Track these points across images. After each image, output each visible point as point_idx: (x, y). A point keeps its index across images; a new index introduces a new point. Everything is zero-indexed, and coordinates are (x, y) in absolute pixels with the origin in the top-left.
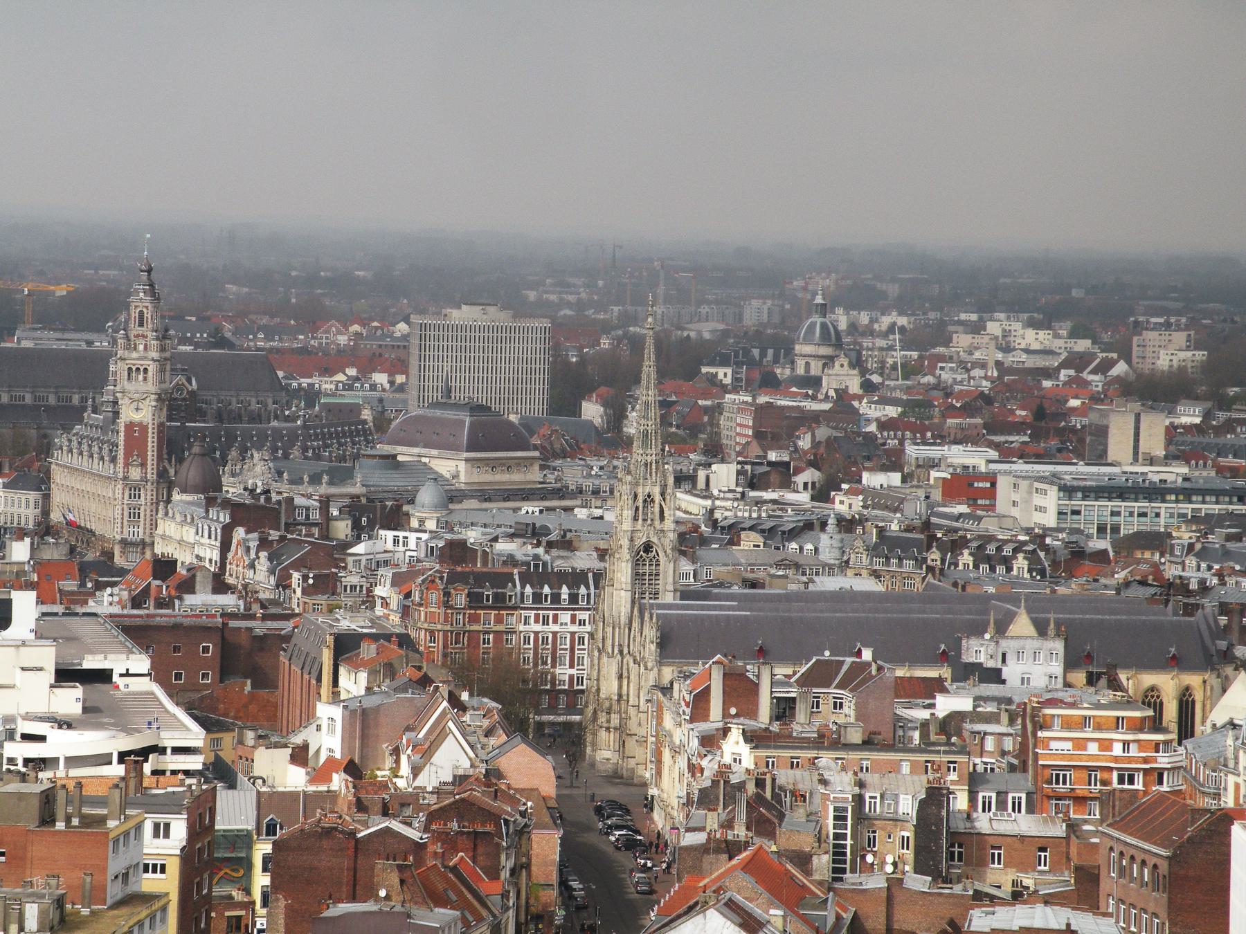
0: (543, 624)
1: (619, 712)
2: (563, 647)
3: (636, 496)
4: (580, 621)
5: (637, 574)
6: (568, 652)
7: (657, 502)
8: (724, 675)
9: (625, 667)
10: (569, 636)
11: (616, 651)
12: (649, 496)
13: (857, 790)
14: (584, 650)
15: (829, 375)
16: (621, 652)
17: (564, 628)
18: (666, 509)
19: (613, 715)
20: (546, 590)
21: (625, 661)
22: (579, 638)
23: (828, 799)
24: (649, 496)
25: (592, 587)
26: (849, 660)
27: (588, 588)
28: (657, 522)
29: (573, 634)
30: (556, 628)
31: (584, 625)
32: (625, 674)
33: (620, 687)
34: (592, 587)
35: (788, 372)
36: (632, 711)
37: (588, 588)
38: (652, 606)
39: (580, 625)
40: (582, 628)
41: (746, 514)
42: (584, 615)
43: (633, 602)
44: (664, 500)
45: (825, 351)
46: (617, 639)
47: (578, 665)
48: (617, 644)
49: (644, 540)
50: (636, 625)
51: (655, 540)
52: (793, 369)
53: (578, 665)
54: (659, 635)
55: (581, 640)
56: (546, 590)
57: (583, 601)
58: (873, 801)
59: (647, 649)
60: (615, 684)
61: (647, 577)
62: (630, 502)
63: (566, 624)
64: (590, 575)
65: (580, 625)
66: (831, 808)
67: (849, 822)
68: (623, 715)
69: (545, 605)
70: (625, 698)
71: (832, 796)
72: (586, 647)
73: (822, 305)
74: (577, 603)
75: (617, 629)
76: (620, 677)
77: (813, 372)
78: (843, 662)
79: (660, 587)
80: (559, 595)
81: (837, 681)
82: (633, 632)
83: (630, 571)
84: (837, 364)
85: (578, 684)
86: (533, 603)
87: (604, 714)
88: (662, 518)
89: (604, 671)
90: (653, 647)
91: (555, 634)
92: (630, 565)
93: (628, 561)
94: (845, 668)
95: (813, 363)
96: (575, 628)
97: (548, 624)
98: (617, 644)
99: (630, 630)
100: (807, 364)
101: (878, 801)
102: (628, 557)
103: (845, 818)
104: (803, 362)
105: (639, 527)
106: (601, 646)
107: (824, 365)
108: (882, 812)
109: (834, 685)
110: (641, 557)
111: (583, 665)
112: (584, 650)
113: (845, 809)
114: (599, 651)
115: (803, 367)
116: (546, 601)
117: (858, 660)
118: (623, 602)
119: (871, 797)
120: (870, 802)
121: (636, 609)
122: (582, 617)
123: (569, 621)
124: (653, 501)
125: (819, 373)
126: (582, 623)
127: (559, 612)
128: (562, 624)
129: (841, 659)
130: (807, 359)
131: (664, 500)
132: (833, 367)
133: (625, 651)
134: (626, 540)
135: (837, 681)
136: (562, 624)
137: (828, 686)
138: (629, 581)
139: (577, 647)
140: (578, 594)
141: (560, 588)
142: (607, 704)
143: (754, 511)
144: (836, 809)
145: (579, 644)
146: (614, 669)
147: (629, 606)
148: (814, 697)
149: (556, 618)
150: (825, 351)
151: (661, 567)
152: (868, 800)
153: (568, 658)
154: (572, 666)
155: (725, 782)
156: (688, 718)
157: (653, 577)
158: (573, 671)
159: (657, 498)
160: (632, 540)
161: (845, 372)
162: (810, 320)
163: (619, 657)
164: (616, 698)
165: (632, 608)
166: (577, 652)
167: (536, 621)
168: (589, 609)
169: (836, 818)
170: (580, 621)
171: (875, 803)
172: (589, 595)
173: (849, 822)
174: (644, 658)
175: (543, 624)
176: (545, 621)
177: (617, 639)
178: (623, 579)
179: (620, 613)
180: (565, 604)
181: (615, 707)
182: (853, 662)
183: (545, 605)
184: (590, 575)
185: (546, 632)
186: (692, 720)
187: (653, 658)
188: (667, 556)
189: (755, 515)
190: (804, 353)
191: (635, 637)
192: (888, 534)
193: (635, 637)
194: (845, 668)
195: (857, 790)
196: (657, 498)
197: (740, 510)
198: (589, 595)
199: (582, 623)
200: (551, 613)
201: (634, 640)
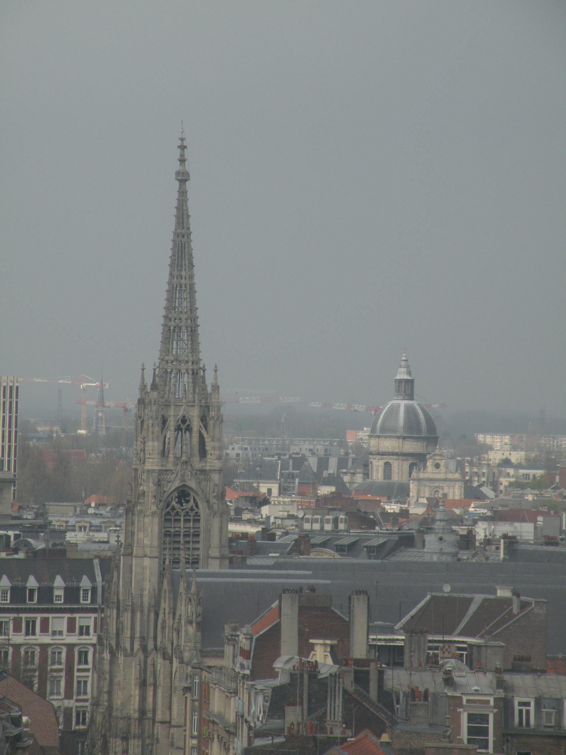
0: (27, 634)
1: (141, 736)
2: (56, 667)
3: (164, 421)
4: (81, 628)
5: (167, 534)
6: (63, 674)
7: (195, 429)
8: (301, 609)
9: (150, 669)
10: (64, 650)
11: (137, 646)
12: (184, 420)
13: (501, 693)
14: (87, 670)
15: (419, 480)
16: (144, 648)
17: (58, 640)
18: (208, 440)
19: (132, 742)
20: (32, 582)
21: (149, 660)
22: (80, 653)
23: (461, 705)
24: (184, 420)
25: (99, 579)
26: (479, 598)
27: (92, 579)
28: (196, 459)
29: (70, 647)
30: (46, 639)
31: (88, 634)
32: (150, 680)
33: (143, 699)
34: (99, 579)
35: (359, 478)
36: (159, 730)
37: (92, 579)
38: (190, 575)
39: (81, 634)
40: (85, 639)
41: (317, 526)
42: (89, 620)
43: (161, 575)
44: (206, 427)
45: (410, 447)
46: (138, 628)
47: (79, 693)
48: (138, 635)
49: (177, 484)
50: (165, 605)
51: (192, 484)
52: (366, 475)
53: (79, 693)
54: (200, 610)
55: (83, 656)
56: (32, 582)
57: (85, 598)
58: (524, 709)
59: (183, 634)
60: (136, 692)
61: (182, 539)
62: (157, 429)
63: (61, 633)
64: (96, 562)
65: (81, 634)
66: (464, 718)
67: (491, 738)
68: (147, 742)
69: (29, 604)
70: (150, 715)
71: (465, 699)
72: (90, 666)
73: (407, 381)
74: (78, 602)
75: (138, 615)
76: (143, 684)
77: (395, 478)
78: (470, 600)
79: (201, 553)
80: (51, 590)
81: (462, 625)
82: (161, 616)
83: (156, 529)
84: (429, 463)
85: (78, 723)
86: (12, 602)
87: (119, 742)
88: (203, 453)
89: (119, 677)
90: (191, 630)
91: (44, 647)
92: (156, 520)
93: (154, 513)
94: (473, 608)
95: (395, 465)
96: (73, 639)
97: (34, 634)
98: (138, 635)
99: (157, 614)
100: (388, 466)
101: (532, 709)
102: (154, 508)
103: (485, 732)
104: (381, 463)
105: (170, 466)
106: (113, 643)
107: (412, 466)
108: (538, 725)
109: (458, 631)
110: (173, 509)
111: (85, 693)
112: (87, 670)
113: (484, 718)
114: (112, 652)
115: (381, 470)
116: (31, 599)
117: (492, 597)
118: (147, 575)
119: (521, 704)
120: (521, 711)
121: (166, 586)
122: (84, 623)
123: (65, 628)
124: (189, 429)
125: (405, 479)
126: (84, 631)
127: (50, 616)
128: (54, 633)
129: (469, 596)
130: (391, 459)
131: (206, 427)
132: (425, 467)
133: (150, 646)
134: (151, 485)
135: (462, 625)
136: (54, 633)
137: (450, 633)
138: (156, 543)
139: (76, 667)
140: (78, 589)
141: (52, 580)
142: (122, 724)
143: (328, 521)
144: (471, 718)
145: (80, 663)
146: (134, 673)
147: (155, 580)
148: (430, 648)
149: (45, 624)
150: (410, 447)
151: (202, 524)
152: (517, 708)
153: (63, 684)
154: (69, 695)
155: (310, 677)
156: (247, 672)
157: (190, 539)
158: (71, 703)
159: (196, 424)
160: (159, 484)
161: (442, 476)
162: (390, 403)
163: (141, 655)
164: (136, 715)
165: (161, 583)
166: (76, 674)
167: (17, 629)
168: (94, 611)
169: (471, 731)
170: (81, 628)
171: (528, 712)
172: (94, 590)
173: (491, 738)
174: (178, 646)
175: (27, 634)
176: (30, 630)
177: (138, 628)
178: (147, 542)
179: (142, 590)
180: (60, 603)
181: (135, 729)
182: (485, 600)
183: (29, 604)
184: (96, 562)
185: (31, 646)
186: (254, 676)
187: (191, 645)
188: (210, 507)
189: (328, 527)
190: (382, 450)
191: (164, 621)
192: (522, 547)
193: (164, 621)
194: (473, 608)
195: (501, 693)
196: (196, 424)
197: (307, 521)
198: (94, 590)
199: (84, 631)
200: (39, 617)
201: (163, 628)
